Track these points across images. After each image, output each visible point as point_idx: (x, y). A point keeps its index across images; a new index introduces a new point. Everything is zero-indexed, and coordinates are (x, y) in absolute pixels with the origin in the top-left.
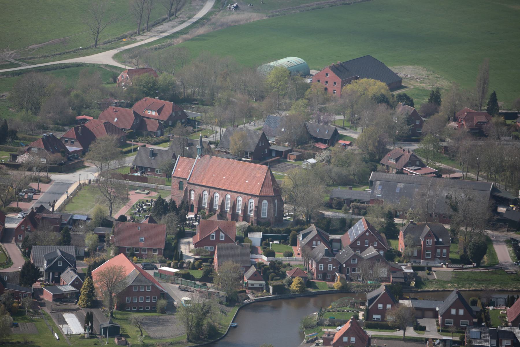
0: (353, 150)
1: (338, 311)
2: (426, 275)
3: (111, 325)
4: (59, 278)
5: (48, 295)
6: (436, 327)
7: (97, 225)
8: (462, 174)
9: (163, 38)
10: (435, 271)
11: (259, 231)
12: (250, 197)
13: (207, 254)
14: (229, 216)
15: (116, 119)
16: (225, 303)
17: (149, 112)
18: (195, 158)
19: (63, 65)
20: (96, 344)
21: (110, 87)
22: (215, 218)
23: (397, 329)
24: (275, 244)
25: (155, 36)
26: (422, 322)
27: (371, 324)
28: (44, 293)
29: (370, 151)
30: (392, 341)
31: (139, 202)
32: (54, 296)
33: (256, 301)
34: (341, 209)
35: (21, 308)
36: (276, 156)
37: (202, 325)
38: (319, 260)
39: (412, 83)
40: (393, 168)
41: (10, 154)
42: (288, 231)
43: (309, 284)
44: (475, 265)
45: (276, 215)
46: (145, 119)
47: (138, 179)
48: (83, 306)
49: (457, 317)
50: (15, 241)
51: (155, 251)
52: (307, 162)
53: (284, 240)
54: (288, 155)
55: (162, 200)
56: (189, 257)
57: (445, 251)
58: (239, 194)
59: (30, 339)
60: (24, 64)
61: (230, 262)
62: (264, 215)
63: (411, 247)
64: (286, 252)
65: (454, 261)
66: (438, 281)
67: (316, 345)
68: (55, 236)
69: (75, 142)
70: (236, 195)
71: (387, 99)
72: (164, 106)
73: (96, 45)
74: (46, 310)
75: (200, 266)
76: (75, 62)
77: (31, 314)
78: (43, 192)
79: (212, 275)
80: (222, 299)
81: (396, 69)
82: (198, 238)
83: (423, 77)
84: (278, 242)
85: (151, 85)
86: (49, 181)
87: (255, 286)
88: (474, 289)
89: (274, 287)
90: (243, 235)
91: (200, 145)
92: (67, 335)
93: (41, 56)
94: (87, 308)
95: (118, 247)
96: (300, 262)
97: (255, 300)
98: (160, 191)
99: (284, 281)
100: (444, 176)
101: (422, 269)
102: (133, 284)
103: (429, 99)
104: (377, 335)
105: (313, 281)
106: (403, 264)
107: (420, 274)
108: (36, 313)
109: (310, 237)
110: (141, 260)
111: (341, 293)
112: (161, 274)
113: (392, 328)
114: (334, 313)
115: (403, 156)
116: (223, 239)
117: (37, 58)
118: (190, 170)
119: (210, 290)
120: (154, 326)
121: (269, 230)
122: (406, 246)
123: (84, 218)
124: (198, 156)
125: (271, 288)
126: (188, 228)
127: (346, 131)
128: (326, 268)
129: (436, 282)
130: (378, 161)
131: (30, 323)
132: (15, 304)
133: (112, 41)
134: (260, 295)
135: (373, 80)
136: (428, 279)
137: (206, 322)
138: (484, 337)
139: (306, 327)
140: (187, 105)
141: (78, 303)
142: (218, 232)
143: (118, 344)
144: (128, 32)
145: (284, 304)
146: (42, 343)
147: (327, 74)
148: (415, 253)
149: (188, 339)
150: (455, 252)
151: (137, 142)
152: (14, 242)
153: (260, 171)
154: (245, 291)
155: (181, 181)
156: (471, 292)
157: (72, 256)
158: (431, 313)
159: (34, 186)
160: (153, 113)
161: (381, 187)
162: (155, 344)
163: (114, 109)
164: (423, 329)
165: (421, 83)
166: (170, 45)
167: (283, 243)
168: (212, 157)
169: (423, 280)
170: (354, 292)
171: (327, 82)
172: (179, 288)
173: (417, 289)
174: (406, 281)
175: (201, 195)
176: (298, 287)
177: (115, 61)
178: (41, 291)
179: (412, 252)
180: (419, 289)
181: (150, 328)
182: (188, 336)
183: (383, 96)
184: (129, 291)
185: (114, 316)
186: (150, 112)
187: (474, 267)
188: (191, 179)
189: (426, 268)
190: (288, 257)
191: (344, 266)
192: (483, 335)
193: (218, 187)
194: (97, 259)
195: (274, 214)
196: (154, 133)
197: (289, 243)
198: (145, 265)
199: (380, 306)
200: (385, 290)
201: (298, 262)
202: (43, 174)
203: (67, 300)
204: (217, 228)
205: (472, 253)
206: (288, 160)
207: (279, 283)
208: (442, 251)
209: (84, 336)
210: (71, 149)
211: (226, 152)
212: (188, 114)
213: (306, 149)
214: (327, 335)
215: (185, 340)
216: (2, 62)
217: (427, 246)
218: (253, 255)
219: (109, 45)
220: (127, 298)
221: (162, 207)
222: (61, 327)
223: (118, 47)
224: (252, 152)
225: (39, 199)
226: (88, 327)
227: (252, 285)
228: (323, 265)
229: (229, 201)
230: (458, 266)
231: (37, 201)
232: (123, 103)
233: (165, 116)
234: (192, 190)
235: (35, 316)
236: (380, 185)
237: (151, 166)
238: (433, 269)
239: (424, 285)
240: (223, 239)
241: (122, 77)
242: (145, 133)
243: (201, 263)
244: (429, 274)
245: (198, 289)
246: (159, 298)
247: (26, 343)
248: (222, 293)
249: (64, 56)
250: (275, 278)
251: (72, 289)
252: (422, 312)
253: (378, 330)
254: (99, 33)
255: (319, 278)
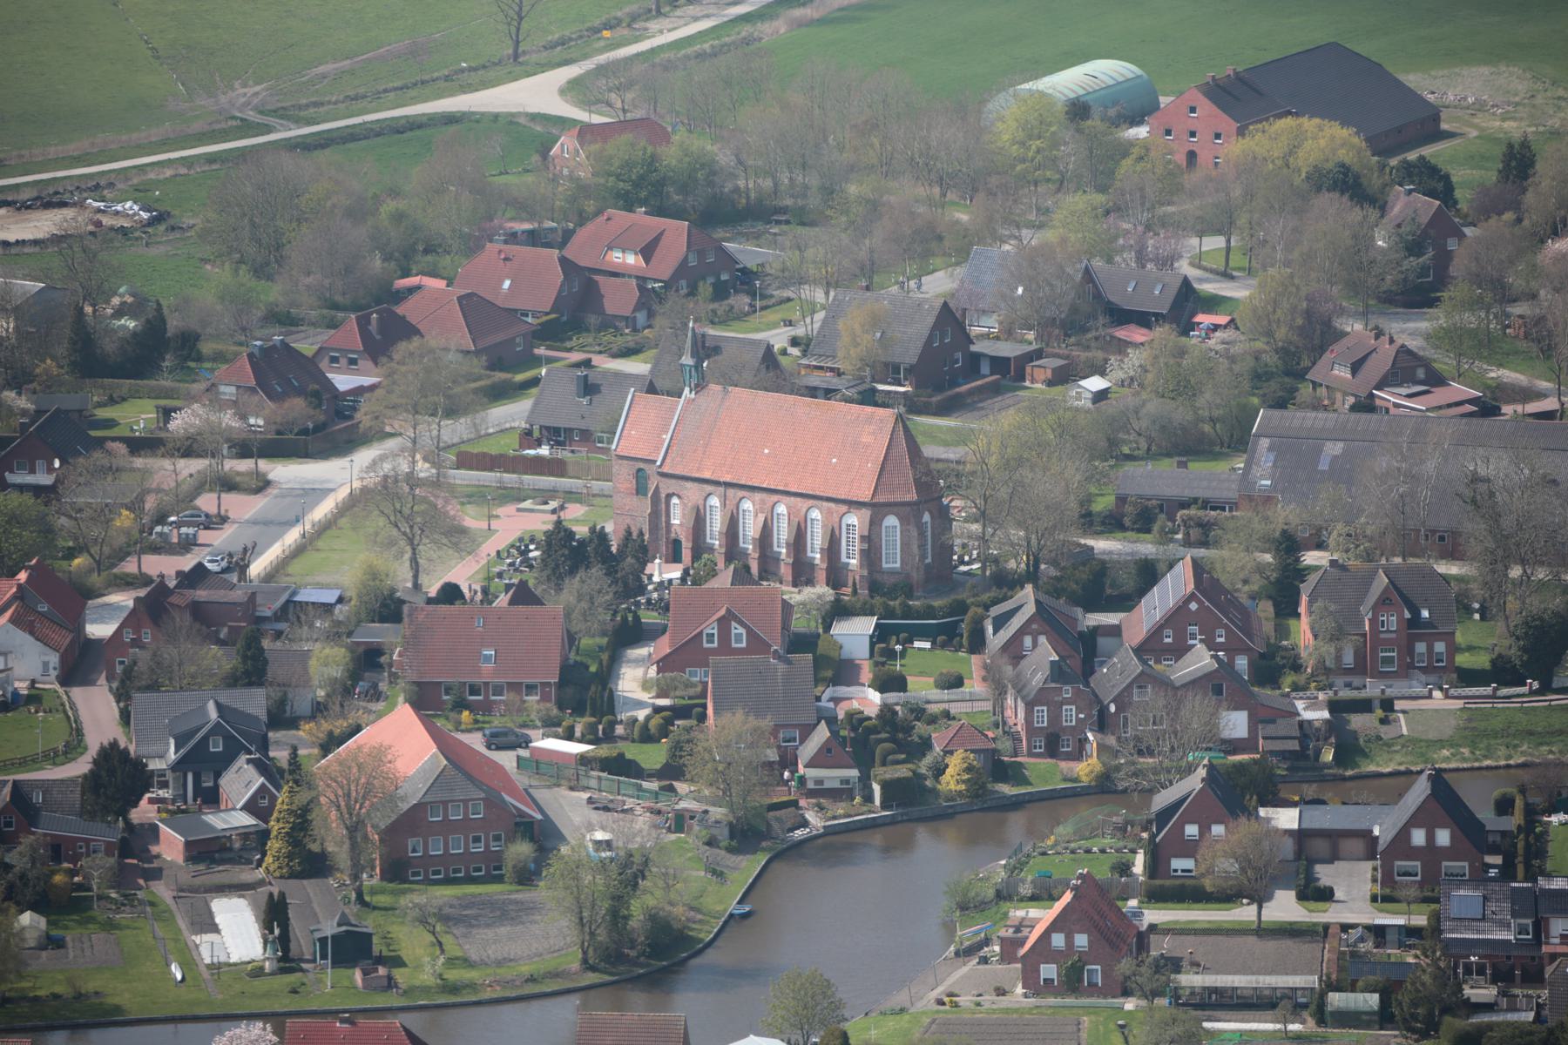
0: (1227, 343)
1: (1073, 852)
2: (1377, 723)
3: (344, 928)
4: (216, 787)
5: (171, 846)
6: (1369, 886)
7: (363, 616)
8: (1556, 399)
9: (731, 21)
10: (1404, 712)
11: (866, 611)
12: (844, 508)
13: (691, 692)
14: (785, 570)
15: (507, 284)
16: (724, 844)
17: (617, 257)
18: (680, 397)
19: (403, 121)
20: (294, 991)
21: (516, 182)
22: (724, 579)
23: (1245, 901)
24: (919, 649)
25: (708, 16)
26: (1325, 874)
27: (1161, 886)
28: (162, 837)
29: (1280, 344)
30: (1220, 938)
31: (521, 540)
32: (189, 845)
33: (829, 832)
34: (1148, 531)
35: (80, 887)
36: (992, 374)
37: (627, 918)
38: (1031, 696)
39: (1476, 121)
40: (1345, 394)
41: (157, 407)
42: (960, 608)
43: (1002, 770)
44: (1536, 685)
45: (929, 560)
46: (597, 278)
47: (539, 466)
48: (277, 874)
49: (1430, 852)
50: (108, 679)
51: (531, 689)
52: (1080, 386)
53: (946, 636)
54: (1028, 369)
55: (566, 530)
56: (640, 704)
57: (1440, 647)
58: (811, 502)
59: (91, 986)
60: (282, 125)
61: (740, 715)
62: (892, 560)
63: (1331, 640)
64: (941, 674)
65: (1469, 677)
66: (1410, 742)
67: (979, 963)
68: (219, 659)
69: (359, 362)
70: (802, 504)
71: (1357, 177)
72: (661, 234)
73: (516, 56)
74: (162, 891)
75: (664, 732)
76: (439, 111)
77: (109, 906)
78: (234, 522)
79: (681, 757)
80: (715, 832)
81: (1435, 78)
82: (663, 646)
83: (1517, 99)
84: (927, 645)
85: (638, 170)
86: (262, 485)
87: (827, 785)
88: (1521, 760)
89: (886, 786)
90: (820, 626)
91: (692, 356)
92: (210, 967)
93: (341, 98)
94: (289, 878)
95: (418, 684)
96: (982, 704)
97: (824, 827)
98: (597, 501)
99: (924, 766)
100: (1507, 409)
101: (1364, 706)
102: (428, 799)
103: (1500, 172)
104: (1176, 922)
105: (1018, 759)
106: (1308, 693)
107: (1357, 721)
108: (129, 900)
109: (1016, 623)
110: (487, 718)
111: (1103, 792)
112: (537, 762)
113: (1227, 897)
114: (1057, 859)
115: (1374, 354)
116: (744, 645)
117: (329, 103)
118: (667, 432)
119: (683, 805)
120: (488, 926)
121: (897, 607)
122: (1316, 637)
123: (329, 597)
124: (687, 390)
125: (876, 788)
126: (656, 614)
127: (1231, 284)
128: (1055, 718)
129: (1403, 746)
130: (1300, 375)
131: (103, 935)
132: (58, 878)
133: (571, 39)
134: (841, 812)
135: (1317, 121)
136: (1379, 738)
137: (637, 910)
138: (1493, 913)
139: (963, 907)
140: (753, 226)
141: (264, 865)
142: (724, 623)
143: (364, 988)
144: (627, 10)
145: (922, 834)
146: (127, 995)
147: (1193, 110)
148: (1349, 659)
149: (585, 961)
150: (1487, 649)
151: (570, 350)
152: (105, 682)
153: (872, 427)
154: (794, 804)
155: (640, 470)
156: (1512, 771)
157: (257, 718)
158: (1358, 846)
159: (207, 502)
160: (631, 259)
161: (1272, 457)
162: (481, 981)
163: (500, 252)
164: (1326, 895)
165: (1504, 120)
166: (747, 42)
167: (943, 646)
168: (730, 388)
169: (1361, 741)
170: (1125, 791)
171: (1193, 134)
172: (590, 801)
173: (1341, 771)
174: (1304, 747)
175: (701, 507)
176: (963, 782)
177: (567, 102)
178: (153, 832)
179: (1338, 658)
180: (1346, 769)
181: (475, 931)
182: (584, 953)
183: (1344, 168)
184: (413, 820)
185: (367, 898)
186: (620, 255)
187: (1532, 693)
188: (668, 460)
189: (1377, 703)
190: (948, 688)
191: (1113, 708)
192: (1492, 907)
193: (750, 483)
194: (339, 726)
195: (923, 556)
196: (627, 318)
197: (961, 646)
198: (494, 735)
199: (1192, 830)
200: (1203, 780)
201: (976, 704)
202: (244, 465)
203: (231, 855)
204: (722, 612)
205: (1524, 649)
206: (1027, 384)
207: (902, 771)
208: (1430, 648)
209: (262, 968)
210: (343, 381)
211: (832, 370)
212: (739, 257)
213: (1088, 348)
214: (1011, 930)
215: (575, 966)
216: (219, 122)
217: (1382, 636)
218: (838, 688)
219: (559, 52)
220: (411, 842)
221: (567, 552)
222: (198, 942)
223: (585, 57)
224: (912, 366)
225: (216, 543)
226: (271, 937)
227: (819, 782)
228: (1045, 708)
229: (784, 524)
230: (1481, 690)
231: (209, 549)
232: (553, 230)
233: (665, 264)
234: (674, 494)
235: (123, 912)
236: (1270, 449)
237: (582, 425)
238: (1398, 705)
239: (1365, 755)
240: (744, 645)
241: (563, 151)
242: (593, 320)
243: (669, 722)
244: (1384, 721)
245: (647, 804)
246: (511, 839)
247: (79, 996)
248: (717, 812)
249: (413, 93)
250: (890, 757)
251: (246, 820)
252: (1334, 844)
253: (1186, 905)
254: (521, 18)
255: (1038, 750)
